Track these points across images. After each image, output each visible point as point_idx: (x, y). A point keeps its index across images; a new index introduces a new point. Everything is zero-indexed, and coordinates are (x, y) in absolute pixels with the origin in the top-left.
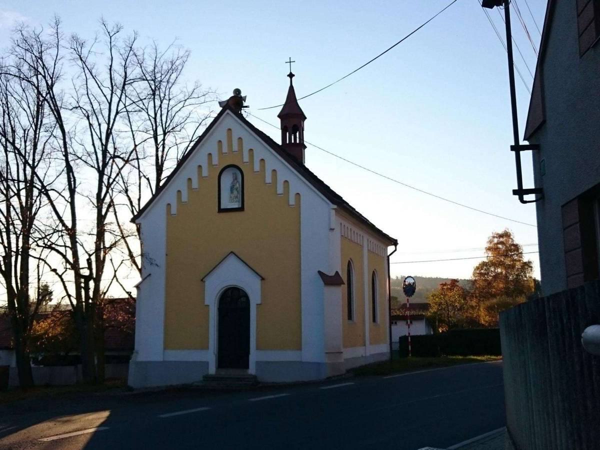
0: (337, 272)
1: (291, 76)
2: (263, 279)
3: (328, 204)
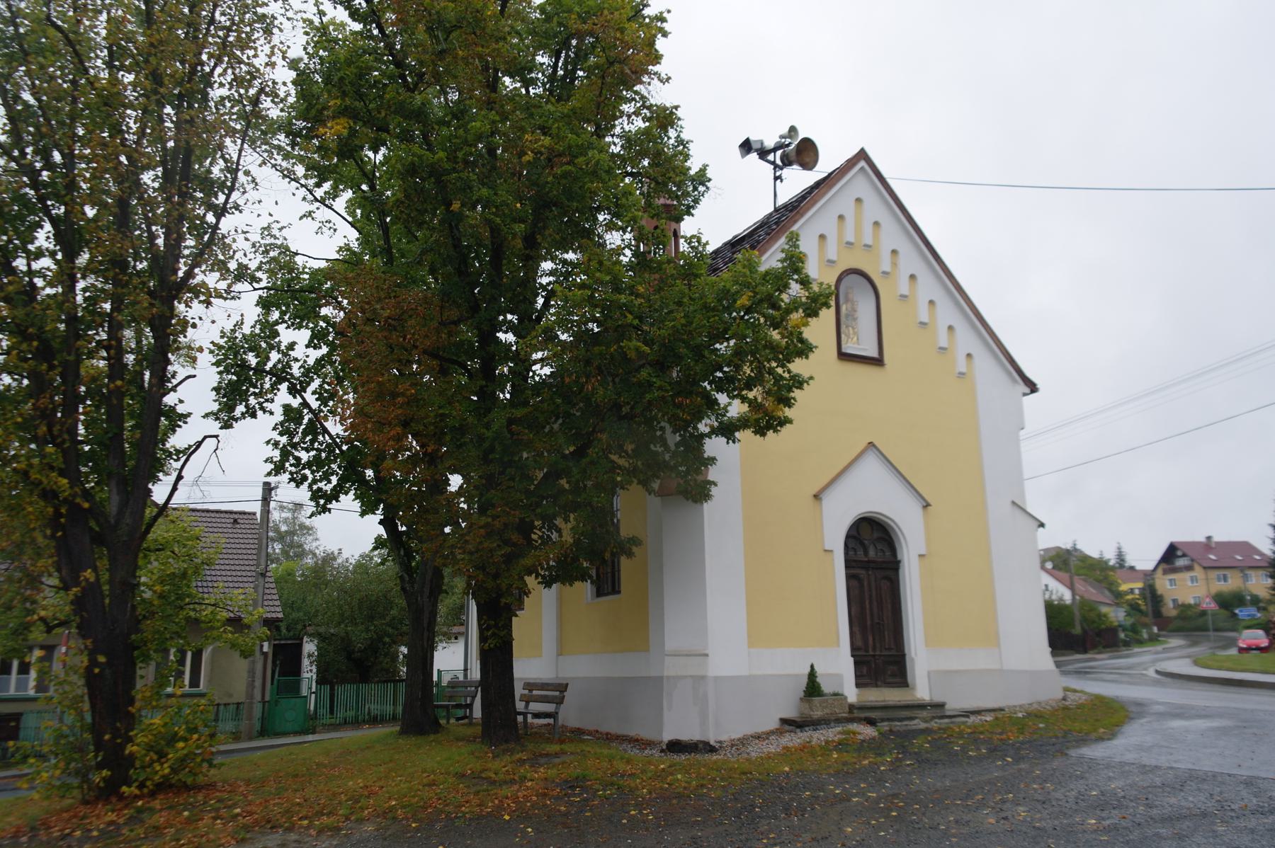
2: (927, 505)
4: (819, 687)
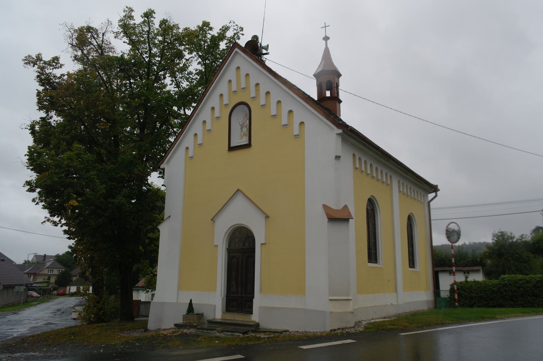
0: (346, 207)
1: (326, 38)
2: (267, 217)
3: (332, 128)
4: (193, 309)
